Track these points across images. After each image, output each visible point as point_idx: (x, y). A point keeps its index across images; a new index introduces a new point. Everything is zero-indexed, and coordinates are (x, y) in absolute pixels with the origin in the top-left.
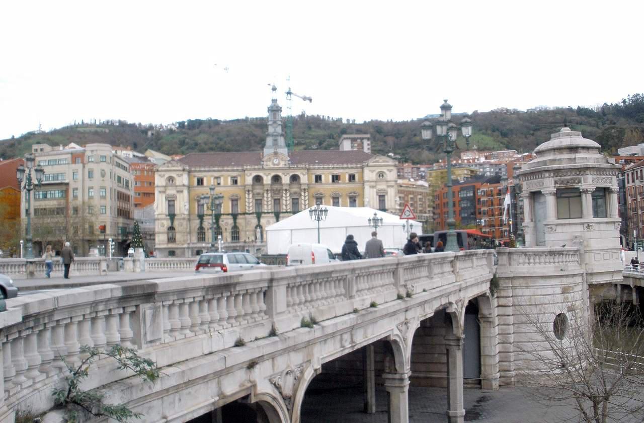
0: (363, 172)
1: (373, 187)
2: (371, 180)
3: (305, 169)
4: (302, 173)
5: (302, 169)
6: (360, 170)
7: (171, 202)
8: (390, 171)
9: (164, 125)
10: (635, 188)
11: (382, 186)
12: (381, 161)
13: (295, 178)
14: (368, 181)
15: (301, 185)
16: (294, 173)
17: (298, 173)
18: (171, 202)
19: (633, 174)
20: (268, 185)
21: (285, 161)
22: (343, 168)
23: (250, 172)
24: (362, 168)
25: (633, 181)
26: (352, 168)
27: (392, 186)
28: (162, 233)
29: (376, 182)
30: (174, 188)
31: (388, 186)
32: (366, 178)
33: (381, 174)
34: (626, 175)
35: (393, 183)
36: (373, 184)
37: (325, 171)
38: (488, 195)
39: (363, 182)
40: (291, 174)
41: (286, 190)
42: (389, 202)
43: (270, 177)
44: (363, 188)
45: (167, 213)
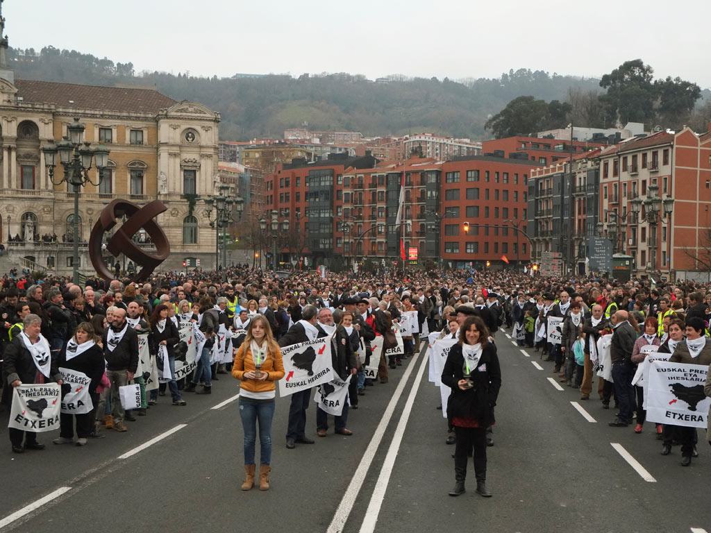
0: (157, 128)
1: (175, 155)
2: (172, 141)
3: (49, 112)
4: (41, 120)
5: (43, 111)
6: (152, 124)
7: (190, 174)
8: (207, 129)
9: (585, 77)
10: (618, 185)
11: (191, 155)
12: (190, 109)
13: (27, 129)
14: (166, 144)
15: (39, 141)
16: (24, 119)
17: (35, 119)
18: (190, 174)
19: (616, 163)
20: (11, 139)
21: (9, 94)
22: (119, 118)
23: (15, 114)
24: (156, 120)
25: (616, 173)
26: (137, 118)
27: (209, 156)
28: (176, 227)
29: (180, 146)
30: (197, 150)
31: (202, 156)
32: (162, 139)
33: (190, 134)
34: (602, 163)
35: (211, 151)
36: (176, 150)
37: (118, 122)
38: (354, 186)
39: (157, 146)
40: (21, 119)
41: (9, 149)
42: (203, 184)
43: (14, 125)
44: (157, 156)
45: (182, 193)
